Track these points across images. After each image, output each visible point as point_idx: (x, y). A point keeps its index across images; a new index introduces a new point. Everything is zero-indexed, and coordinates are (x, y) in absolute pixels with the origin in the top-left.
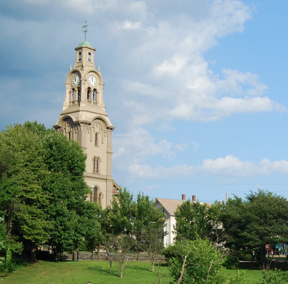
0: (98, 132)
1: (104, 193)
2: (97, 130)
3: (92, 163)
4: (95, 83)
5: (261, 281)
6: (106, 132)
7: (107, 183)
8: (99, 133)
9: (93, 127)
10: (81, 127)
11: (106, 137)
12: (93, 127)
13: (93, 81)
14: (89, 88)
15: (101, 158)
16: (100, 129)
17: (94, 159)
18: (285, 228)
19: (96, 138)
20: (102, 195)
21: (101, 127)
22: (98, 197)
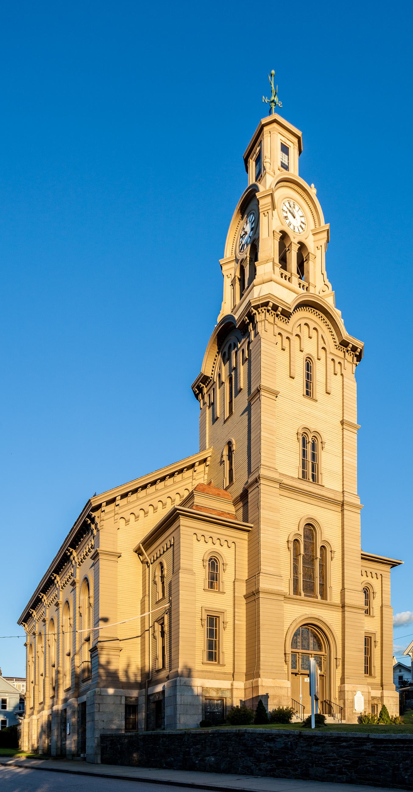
0: (315, 355)
1: (336, 545)
2: (310, 347)
3: (297, 447)
4: (303, 226)
5: (16, 684)
6: (337, 360)
7: (343, 515)
8: (316, 358)
9: (297, 335)
10: (259, 325)
11: (339, 376)
12: (297, 335)
13: (294, 217)
14: (284, 236)
15: (325, 437)
16: (320, 348)
17: (304, 439)
18: (2, 768)
19: (308, 374)
20: (328, 549)
21: (322, 342)
22: (318, 555)
